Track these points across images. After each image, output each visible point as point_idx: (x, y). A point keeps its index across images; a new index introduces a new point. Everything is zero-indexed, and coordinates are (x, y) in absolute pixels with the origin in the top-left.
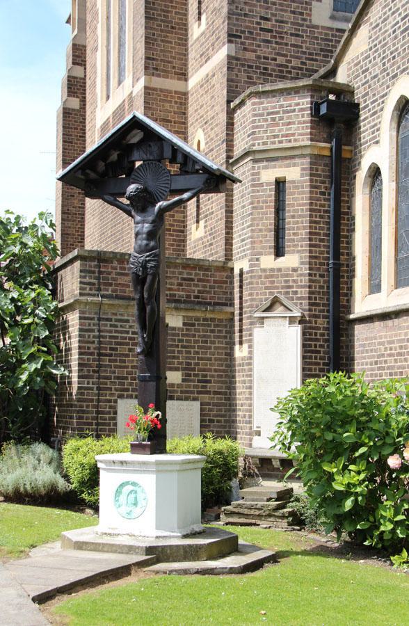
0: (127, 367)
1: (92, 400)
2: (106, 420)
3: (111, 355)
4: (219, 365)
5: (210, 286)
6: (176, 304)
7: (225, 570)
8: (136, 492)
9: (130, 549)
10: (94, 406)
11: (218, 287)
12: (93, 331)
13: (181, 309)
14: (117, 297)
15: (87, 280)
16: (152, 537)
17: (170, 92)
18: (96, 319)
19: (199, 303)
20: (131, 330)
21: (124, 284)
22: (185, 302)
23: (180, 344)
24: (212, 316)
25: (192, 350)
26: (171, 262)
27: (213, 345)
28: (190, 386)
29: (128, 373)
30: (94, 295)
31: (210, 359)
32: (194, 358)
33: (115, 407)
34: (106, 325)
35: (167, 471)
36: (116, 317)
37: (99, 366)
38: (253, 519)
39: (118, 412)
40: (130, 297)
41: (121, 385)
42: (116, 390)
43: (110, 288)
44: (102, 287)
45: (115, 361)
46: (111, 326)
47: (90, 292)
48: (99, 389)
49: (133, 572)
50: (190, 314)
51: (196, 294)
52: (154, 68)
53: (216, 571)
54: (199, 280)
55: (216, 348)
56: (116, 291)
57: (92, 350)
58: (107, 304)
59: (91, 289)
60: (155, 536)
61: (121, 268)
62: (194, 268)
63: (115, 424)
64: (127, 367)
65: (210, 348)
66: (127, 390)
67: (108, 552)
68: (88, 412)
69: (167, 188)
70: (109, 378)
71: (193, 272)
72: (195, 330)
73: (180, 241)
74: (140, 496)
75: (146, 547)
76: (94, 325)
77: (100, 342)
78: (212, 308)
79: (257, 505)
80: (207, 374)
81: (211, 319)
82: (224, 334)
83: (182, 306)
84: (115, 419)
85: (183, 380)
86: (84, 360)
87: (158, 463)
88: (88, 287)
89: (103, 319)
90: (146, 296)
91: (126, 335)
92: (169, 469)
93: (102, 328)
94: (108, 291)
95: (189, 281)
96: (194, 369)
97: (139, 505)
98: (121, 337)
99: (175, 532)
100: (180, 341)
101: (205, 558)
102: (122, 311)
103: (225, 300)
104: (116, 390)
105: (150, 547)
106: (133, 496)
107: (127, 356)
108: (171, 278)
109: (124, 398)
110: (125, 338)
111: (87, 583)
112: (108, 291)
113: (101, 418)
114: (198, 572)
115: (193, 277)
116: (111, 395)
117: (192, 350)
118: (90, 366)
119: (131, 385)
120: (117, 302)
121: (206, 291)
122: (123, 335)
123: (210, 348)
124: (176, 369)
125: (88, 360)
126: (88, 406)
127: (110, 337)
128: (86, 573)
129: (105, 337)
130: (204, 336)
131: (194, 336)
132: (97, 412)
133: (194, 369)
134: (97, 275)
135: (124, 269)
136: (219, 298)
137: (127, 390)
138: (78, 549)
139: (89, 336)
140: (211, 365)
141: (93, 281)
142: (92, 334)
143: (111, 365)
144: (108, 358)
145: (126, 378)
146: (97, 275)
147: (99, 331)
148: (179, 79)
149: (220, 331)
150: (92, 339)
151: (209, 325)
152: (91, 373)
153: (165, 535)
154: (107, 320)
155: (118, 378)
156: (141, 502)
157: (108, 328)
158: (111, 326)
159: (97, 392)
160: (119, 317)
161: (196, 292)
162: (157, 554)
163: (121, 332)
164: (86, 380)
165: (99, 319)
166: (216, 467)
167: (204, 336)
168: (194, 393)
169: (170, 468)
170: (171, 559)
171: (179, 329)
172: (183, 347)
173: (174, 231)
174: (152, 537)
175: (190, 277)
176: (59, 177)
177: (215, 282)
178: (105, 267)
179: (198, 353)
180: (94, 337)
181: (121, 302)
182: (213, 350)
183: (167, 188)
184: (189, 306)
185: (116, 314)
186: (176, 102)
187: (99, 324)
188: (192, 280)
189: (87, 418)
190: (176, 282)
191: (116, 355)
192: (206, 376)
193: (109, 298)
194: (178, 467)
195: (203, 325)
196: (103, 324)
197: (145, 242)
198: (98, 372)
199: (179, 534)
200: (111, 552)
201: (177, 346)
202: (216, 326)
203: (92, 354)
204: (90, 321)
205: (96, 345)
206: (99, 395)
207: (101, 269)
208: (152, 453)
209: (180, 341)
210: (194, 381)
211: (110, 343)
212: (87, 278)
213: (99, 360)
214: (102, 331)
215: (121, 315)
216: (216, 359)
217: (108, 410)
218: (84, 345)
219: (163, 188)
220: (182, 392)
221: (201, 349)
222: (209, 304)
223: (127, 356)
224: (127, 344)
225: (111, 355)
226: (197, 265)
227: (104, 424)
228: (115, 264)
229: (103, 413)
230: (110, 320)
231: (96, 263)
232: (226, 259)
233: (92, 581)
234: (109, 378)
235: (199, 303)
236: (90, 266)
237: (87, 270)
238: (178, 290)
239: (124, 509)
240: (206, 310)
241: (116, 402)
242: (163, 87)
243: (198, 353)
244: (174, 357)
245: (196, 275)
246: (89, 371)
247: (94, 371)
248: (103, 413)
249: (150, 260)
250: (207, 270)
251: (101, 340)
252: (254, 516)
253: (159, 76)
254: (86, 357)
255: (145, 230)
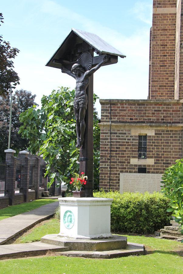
0: (125, 157)
1: (107, 174)
2: (114, 183)
3: (117, 151)
4: (175, 155)
5: (170, 113)
6: (150, 124)
7: (98, 256)
8: (71, 216)
9: (59, 243)
10: (108, 177)
11: (175, 114)
12: (107, 139)
13: (153, 126)
14: (120, 122)
15: (105, 114)
16: (75, 238)
17: (167, 14)
18: (109, 133)
19: (164, 123)
20: (127, 138)
21: (124, 115)
22: (156, 122)
23: (153, 144)
24: (171, 129)
25: (160, 147)
26: (148, 103)
27: (172, 145)
28: (159, 166)
29: (125, 160)
30: (108, 122)
31: (170, 152)
32: (161, 152)
33: (119, 177)
34: (114, 136)
35: (84, 205)
36: (119, 132)
37: (111, 156)
38: (174, 236)
39: (120, 179)
40: (127, 121)
41: (122, 166)
42: (119, 168)
43: (116, 118)
44: (112, 117)
45: (119, 154)
46: (117, 136)
47: (106, 120)
48: (110, 168)
49: (47, 254)
50: (159, 128)
51: (162, 118)
52: (158, 4)
53: (93, 256)
54: (164, 111)
55: (173, 146)
56: (119, 119)
57: (107, 149)
58: (114, 125)
59: (106, 119)
60: (76, 237)
61: (122, 107)
62: (161, 105)
63: (119, 186)
64: (125, 157)
65: (170, 146)
66: (125, 168)
67: (51, 244)
68: (105, 180)
69: (90, 64)
70: (116, 162)
71: (161, 107)
72: (162, 137)
73: (171, 91)
74: (73, 217)
75: (65, 242)
76: (108, 136)
77: (111, 145)
78: (170, 125)
79: (175, 228)
80: (168, 160)
81: (171, 130)
82: (178, 138)
83: (154, 124)
84: (119, 183)
85: (155, 163)
86: (103, 154)
87: (78, 201)
88: (105, 118)
89: (113, 133)
90: (79, 119)
91: (124, 141)
92: (85, 204)
93: (112, 138)
94: (115, 119)
95: (158, 111)
96: (161, 157)
97: (72, 223)
98: (122, 142)
99: (87, 236)
100: (153, 143)
101: (96, 250)
102: (122, 128)
103: (179, 120)
104: (119, 168)
105: (67, 242)
106: (69, 218)
107: (125, 151)
108: (148, 110)
109: (123, 172)
110: (124, 142)
111: (12, 256)
112: (115, 119)
113: (112, 183)
114: (83, 256)
115: (161, 109)
116: (117, 171)
117: (160, 147)
118: (106, 156)
119: (127, 166)
120: (119, 124)
121: (168, 116)
122: (123, 141)
123: (170, 146)
124: (151, 157)
125: (105, 153)
126: (105, 177)
127: (117, 142)
128: (6, 247)
129: (114, 142)
130: (167, 140)
131: (161, 140)
132: (110, 180)
133: (161, 157)
134: (110, 111)
135: (124, 107)
136: (175, 120)
137: (125, 168)
138: (42, 242)
139: (106, 142)
140: (170, 155)
141: (107, 114)
142: (107, 141)
143: (117, 156)
144: (115, 152)
145: (125, 162)
146: (112, 112)
147: (111, 139)
148: (172, 7)
149: (175, 137)
150: (107, 143)
151: (170, 134)
152: (107, 160)
153: (81, 237)
154: (115, 133)
155: (120, 162)
156: (73, 221)
157: (115, 138)
158: (117, 136)
159: (110, 169)
160: (121, 132)
161: (162, 117)
162: (69, 246)
163: (122, 139)
164: (104, 164)
165: (111, 133)
166: (161, 208)
167: (167, 140)
168: (161, 170)
169: (85, 204)
170: (77, 249)
171: (153, 136)
172: (155, 146)
173: (168, 86)
174: (75, 238)
175: (159, 109)
176: (46, 64)
177: (173, 111)
178: (114, 107)
179: (163, 149)
180: (108, 142)
181: (121, 124)
182: (172, 147)
183: (90, 64)
184: (157, 124)
185: (119, 130)
186: (170, 19)
187: (111, 136)
188: (160, 111)
189: (105, 182)
190: (151, 112)
191: (119, 151)
192: (168, 161)
193: (115, 122)
194: (89, 204)
195: (166, 134)
196: (112, 136)
197: (79, 92)
198: (110, 159)
199: (89, 238)
200: (53, 244)
201: (152, 145)
202: (173, 134)
203: (107, 151)
204: (106, 135)
205: (109, 146)
206: (110, 171)
207: (112, 109)
208: (81, 197)
209: (153, 143)
210: (161, 163)
211: (116, 145)
212: (105, 113)
213: (110, 154)
214: (112, 139)
215: (122, 131)
216: (173, 152)
217: (115, 178)
218: (103, 146)
219: (89, 64)
220: (154, 169)
221: (165, 146)
222: (170, 123)
223: (125, 151)
224: (125, 145)
225: (117, 151)
226: (163, 103)
227: (113, 185)
228: (119, 105)
229: (113, 180)
230: (116, 133)
231: (109, 106)
232: (179, 99)
233: (16, 256)
234: (116, 162)
235: (164, 123)
236: (106, 107)
237: (105, 109)
238: (152, 116)
239: (67, 224)
240: (167, 126)
241: (119, 174)
242: (163, 13)
243: (163, 149)
244: (150, 151)
245: (162, 108)
246: (105, 159)
247: (108, 159)
248: (113, 180)
249: (80, 101)
250: (168, 105)
251: (112, 143)
252: (175, 234)
253: (161, 7)
254: (104, 152)
255: (79, 86)
